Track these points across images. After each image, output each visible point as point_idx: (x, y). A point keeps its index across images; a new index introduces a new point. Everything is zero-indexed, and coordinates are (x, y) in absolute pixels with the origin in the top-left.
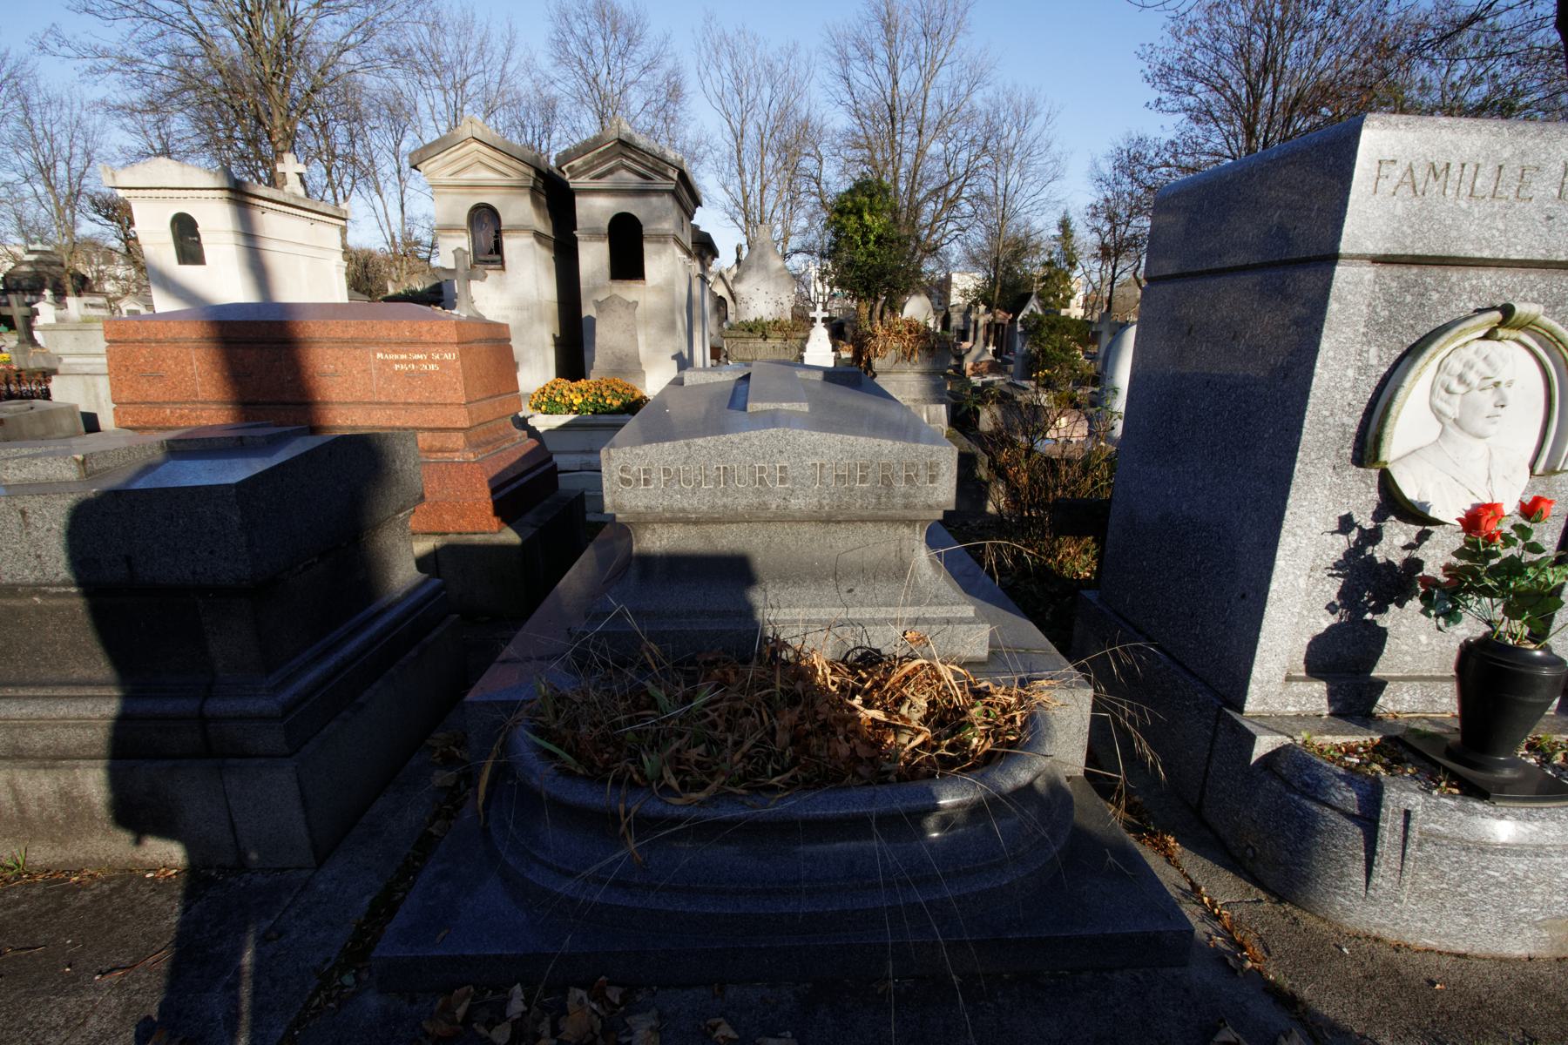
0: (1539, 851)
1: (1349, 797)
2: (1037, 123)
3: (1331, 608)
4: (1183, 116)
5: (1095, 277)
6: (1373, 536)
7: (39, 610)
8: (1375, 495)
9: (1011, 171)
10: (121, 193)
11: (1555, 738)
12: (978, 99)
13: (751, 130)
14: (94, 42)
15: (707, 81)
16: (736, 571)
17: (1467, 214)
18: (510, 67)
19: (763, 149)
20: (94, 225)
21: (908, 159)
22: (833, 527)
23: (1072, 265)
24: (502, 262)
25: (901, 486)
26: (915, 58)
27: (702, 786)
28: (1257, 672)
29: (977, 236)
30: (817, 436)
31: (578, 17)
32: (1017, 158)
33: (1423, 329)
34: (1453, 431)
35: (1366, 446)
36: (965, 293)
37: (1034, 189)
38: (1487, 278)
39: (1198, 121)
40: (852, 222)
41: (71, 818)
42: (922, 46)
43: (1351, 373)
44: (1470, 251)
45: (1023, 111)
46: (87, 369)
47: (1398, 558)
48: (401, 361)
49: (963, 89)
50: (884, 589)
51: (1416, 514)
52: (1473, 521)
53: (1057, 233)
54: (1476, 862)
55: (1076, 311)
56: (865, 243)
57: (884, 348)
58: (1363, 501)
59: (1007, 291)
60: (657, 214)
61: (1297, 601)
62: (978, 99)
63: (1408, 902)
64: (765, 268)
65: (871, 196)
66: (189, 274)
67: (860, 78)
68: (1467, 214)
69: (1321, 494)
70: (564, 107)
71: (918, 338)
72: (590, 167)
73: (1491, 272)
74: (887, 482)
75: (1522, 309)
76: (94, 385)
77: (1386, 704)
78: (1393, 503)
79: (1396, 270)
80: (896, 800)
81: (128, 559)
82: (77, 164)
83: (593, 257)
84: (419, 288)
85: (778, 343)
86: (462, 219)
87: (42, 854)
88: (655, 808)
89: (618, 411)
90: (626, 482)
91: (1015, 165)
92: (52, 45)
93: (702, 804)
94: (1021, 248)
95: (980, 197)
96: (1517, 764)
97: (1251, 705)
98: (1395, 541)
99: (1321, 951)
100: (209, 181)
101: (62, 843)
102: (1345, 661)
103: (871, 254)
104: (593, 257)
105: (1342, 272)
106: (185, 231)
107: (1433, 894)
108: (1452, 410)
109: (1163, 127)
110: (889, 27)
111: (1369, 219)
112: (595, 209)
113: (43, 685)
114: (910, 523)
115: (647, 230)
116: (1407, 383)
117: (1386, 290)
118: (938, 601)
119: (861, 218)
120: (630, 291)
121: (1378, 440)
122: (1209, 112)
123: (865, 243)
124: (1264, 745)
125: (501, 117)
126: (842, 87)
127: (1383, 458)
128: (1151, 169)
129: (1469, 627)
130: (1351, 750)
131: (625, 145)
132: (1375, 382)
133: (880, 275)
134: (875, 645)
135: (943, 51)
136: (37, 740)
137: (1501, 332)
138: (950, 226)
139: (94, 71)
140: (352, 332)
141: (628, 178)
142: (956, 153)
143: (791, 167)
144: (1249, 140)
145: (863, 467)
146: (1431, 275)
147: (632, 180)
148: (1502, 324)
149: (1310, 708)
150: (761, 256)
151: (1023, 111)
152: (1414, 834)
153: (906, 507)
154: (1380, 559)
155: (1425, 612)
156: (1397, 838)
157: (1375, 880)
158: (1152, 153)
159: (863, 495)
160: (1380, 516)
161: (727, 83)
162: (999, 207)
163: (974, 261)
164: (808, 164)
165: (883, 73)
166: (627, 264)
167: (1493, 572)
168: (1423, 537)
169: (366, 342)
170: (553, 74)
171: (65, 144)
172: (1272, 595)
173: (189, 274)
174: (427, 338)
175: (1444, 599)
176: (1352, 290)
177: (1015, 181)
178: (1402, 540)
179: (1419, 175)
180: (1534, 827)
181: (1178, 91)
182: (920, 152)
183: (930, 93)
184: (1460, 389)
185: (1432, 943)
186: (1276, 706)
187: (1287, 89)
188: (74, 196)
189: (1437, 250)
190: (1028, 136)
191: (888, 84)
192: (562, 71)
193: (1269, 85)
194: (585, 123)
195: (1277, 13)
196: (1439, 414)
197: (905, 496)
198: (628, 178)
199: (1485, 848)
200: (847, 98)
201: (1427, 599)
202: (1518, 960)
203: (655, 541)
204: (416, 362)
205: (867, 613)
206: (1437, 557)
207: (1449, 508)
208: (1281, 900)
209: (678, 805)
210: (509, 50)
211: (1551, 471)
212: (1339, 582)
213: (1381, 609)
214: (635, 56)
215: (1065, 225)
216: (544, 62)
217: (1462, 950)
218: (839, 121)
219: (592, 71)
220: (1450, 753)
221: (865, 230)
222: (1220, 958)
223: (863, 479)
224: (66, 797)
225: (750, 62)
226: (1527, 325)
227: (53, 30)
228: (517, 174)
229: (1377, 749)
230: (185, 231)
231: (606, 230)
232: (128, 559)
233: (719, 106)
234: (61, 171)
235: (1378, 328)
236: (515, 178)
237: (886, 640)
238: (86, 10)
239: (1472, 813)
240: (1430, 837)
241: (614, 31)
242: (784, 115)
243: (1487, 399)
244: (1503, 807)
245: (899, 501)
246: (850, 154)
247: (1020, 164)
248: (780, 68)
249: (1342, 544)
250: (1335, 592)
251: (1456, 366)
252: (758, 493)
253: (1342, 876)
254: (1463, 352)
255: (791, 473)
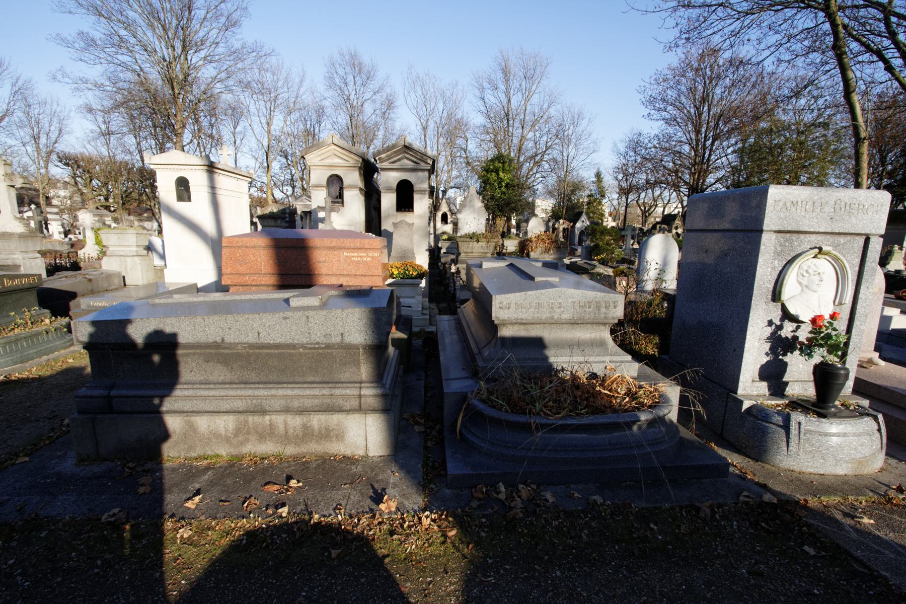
0: (845, 435)
1: (779, 419)
2: (584, 123)
3: (767, 354)
4: (662, 122)
5: (615, 203)
6: (780, 327)
7: (300, 354)
8: (780, 312)
9: (571, 147)
10: (152, 167)
11: (851, 402)
12: (552, 111)
13: (431, 125)
14: (82, 75)
15: (408, 99)
16: (538, 343)
17: (804, 217)
18: (302, 90)
19: (439, 135)
20: (58, 169)
21: (516, 141)
22: (575, 326)
23: (603, 196)
24: (343, 202)
25: (603, 310)
26: (520, 89)
27: (559, 413)
28: (742, 378)
29: (552, 180)
30: (573, 291)
31: (340, 65)
32: (574, 141)
33: (793, 254)
34: (806, 290)
35: (776, 295)
36: (545, 211)
37: (583, 157)
38: (813, 238)
39: (670, 125)
40: (493, 176)
41: (304, 435)
42: (524, 83)
43: (769, 269)
44: (806, 229)
45: (576, 117)
46: (121, 253)
47: (790, 336)
48: (355, 256)
49: (546, 106)
50: (596, 350)
51: (794, 319)
52: (814, 321)
53: (594, 179)
54: (824, 439)
55: (609, 223)
56: (500, 187)
57: (536, 247)
58: (776, 315)
59: (567, 209)
60: (420, 182)
61: (755, 352)
62: (552, 111)
63: (802, 456)
64: (473, 206)
65: (503, 163)
66: (182, 207)
67: (491, 99)
68: (804, 217)
69: (761, 312)
70: (329, 111)
71: (552, 242)
72: (389, 158)
73: (814, 235)
74: (598, 307)
75: (825, 248)
76: (125, 262)
77: (789, 391)
78: (787, 315)
79: (783, 235)
80: (622, 418)
81: (342, 334)
82: (53, 136)
83: (388, 201)
84: (275, 210)
85: (484, 244)
86: (325, 183)
87: (290, 450)
88: (544, 421)
89: (416, 277)
90: (501, 308)
91: (572, 144)
92: (59, 77)
93: (560, 419)
94: (577, 187)
95: (555, 160)
96: (836, 407)
97: (740, 391)
98: (788, 330)
99: (774, 475)
100: (199, 161)
101: (299, 445)
102: (773, 374)
103: (504, 193)
104: (388, 201)
105: (765, 236)
106: (183, 187)
107: (810, 452)
108: (805, 282)
109: (652, 128)
110: (506, 72)
111: (772, 219)
112: (388, 179)
113: (297, 383)
114: (604, 324)
115: (416, 187)
116: (789, 273)
117: (779, 242)
118: (616, 354)
119: (498, 174)
120: (407, 217)
121: (780, 293)
122: (675, 120)
123: (500, 187)
124: (746, 405)
125: (295, 116)
126: (481, 103)
127: (782, 299)
128: (646, 149)
129: (817, 359)
130: (778, 406)
131: (407, 148)
132: (777, 272)
133: (508, 204)
134: (595, 371)
135: (534, 87)
136: (296, 404)
137: (819, 256)
138: (538, 175)
139: (77, 89)
140: (334, 244)
141: (408, 163)
142: (541, 137)
143: (451, 144)
144: (697, 136)
145: (589, 303)
146: (794, 237)
147: (409, 164)
148: (819, 253)
149: (762, 392)
150: (471, 201)
151: (576, 117)
152: (802, 430)
153: (605, 318)
154: (783, 336)
155: (801, 355)
156: (797, 432)
157: (790, 448)
158: (646, 141)
159: (590, 313)
160: (782, 320)
161: (419, 100)
162: (561, 165)
163: (550, 193)
164: (460, 142)
165: (503, 97)
166: (405, 201)
167: (822, 338)
168: (798, 327)
169: (340, 248)
170: (327, 94)
171: (47, 125)
172: (746, 349)
173: (182, 207)
174: (367, 246)
175: (807, 349)
176: (768, 242)
177: (572, 153)
178: (791, 329)
179: (788, 205)
180: (842, 427)
181: (659, 110)
182: (523, 138)
183: (528, 107)
184: (807, 275)
185: (812, 471)
186: (749, 392)
187: (716, 110)
188: (49, 153)
189: (796, 229)
190: (579, 129)
191: (505, 102)
192: (331, 93)
193: (706, 108)
194: (340, 119)
195: (709, 73)
196: (800, 283)
197: (605, 313)
198: (408, 163)
199: (827, 435)
200: (483, 109)
201: (801, 349)
202: (841, 476)
203: (506, 332)
204: (361, 257)
205: (591, 359)
206: (804, 334)
207: (806, 316)
208: (757, 461)
209: (552, 420)
210: (301, 82)
211: (840, 304)
212: (769, 344)
213: (785, 355)
214: (371, 86)
215: (598, 175)
216: (321, 88)
217: (822, 472)
218: (477, 120)
219: (346, 92)
220: (813, 405)
221: (501, 180)
222: (740, 476)
223: (590, 307)
224: (305, 426)
225: (432, 90)
226: (827, 254)
227: (61, 69)
228: (354, 160)
229: (787, 405)
230: (183, 187)
231: (395, 186)
232: (342, 334)
233: (414, 111)
234: (43, 140)
235: (778, 254)
236: (352, 162)
237: (598, 370)
238: (81, 60)
239: (821, 422)
240: (807, 431)
241: (360, 72)
242: (449, 117)
243: (817, 278)
244: (832, 420)
245: (602, 316)
246: (483, 137)
247: (576, 145)
248: (448, 94)
249: (769, 330)
250: (768, 348)
251: (805, 268)
252: (550, 312)
253: (778, 448)
254: (807, 262)
255: (563, 305)
